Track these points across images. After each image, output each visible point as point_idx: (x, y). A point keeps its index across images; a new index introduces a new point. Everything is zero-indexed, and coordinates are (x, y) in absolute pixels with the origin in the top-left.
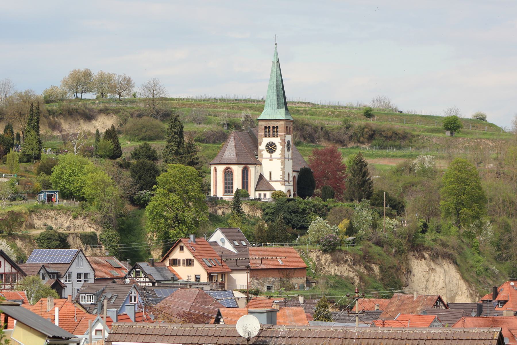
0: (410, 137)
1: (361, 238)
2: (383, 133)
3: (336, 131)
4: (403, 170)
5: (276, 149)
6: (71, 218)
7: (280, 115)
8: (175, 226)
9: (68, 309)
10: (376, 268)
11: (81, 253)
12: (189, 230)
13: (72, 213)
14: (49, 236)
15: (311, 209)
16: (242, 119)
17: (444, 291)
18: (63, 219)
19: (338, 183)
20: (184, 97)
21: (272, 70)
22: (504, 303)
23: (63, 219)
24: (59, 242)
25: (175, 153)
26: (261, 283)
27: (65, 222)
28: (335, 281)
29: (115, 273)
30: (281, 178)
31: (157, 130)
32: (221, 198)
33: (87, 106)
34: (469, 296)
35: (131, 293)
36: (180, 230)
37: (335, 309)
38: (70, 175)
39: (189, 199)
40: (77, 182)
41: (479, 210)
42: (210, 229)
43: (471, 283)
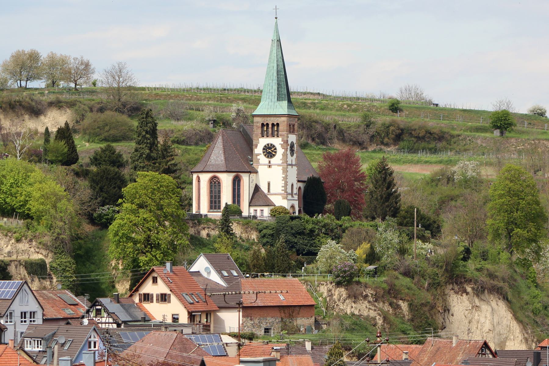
0: (449, 138)
1: (384, 267)
2: (413, 132)
4: (439, 180)
5: (276, 152)
6: (13, 241)
8: (147, 252)
10: (404, 306)
13: (15, 235)
15: (321, 230)
16: (233, 114)
17: (491, 335)
19: (356, 196)
20: (158, 86)
25: (147, 157)
26: (257, 324)
27: (6, 246)
28: (351, 321)
29: (69, 312)
30: (282, 190)
31: (123, 128)
32: (206, 215)
33: (34, 97)
35: (90, 337)
36: (153, 256)
39: (164, 217)
42: (192, 255)
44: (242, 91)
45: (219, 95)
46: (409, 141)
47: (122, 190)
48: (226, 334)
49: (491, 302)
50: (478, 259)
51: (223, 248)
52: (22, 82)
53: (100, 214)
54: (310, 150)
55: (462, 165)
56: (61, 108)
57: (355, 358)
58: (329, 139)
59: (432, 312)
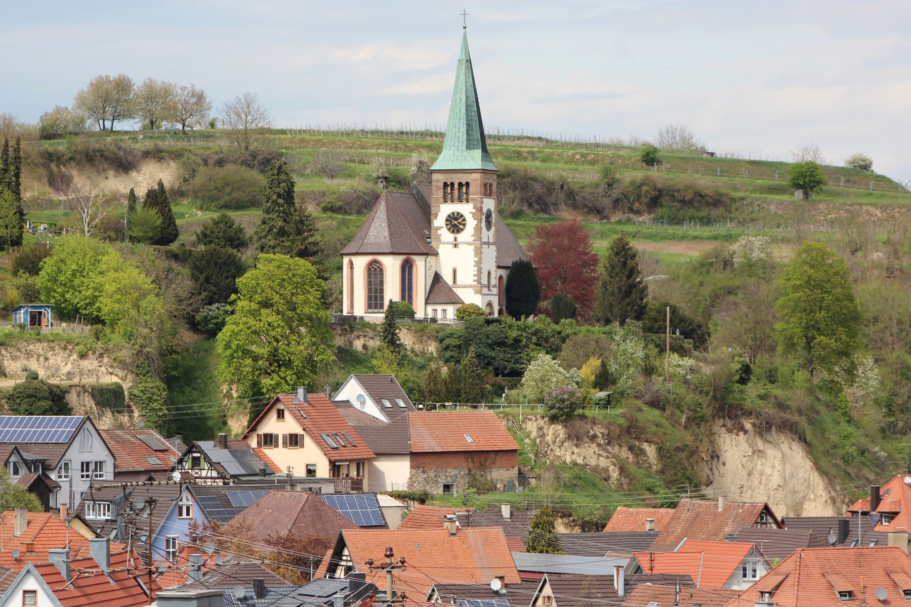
0: (728, 202)
1: (622, 394)
2: (676, 194)
3: (588, 190)
4: (711, 264)
5: (464, 225)
6: (75, 356)
7: (472, 162)
8: (273, 372)
9: (55, 531)
10: (650, 450)
11: (88, 424)
12: (298, 378)
13: (77, 348)
14: (31, 392)
15: (531, 339)
16: (413, 169)
17: (781, 494)
18: (59, 359)
19: (584, 289)
20: (304, 128)
21: (458, 77)
22: (891, 516)
23: (59, 359)
24: (50, 402)
25: (279, 232)
26: (432, 479)
27: (64, 364)
28: (572, 474)
29: (154, 461)
30: (475, 281)
31: (252, 188)
32: (362, 318)
33: (122, 144)
34: (829, 501)
35: (181, 500)
36: (282, 378)
37: (573, 527)
38: (74, 275)
39: (298, 321)
40: (88, 289)
41: (848, 340)
42: (339, 376)
43: (833, 478)
44: (427, 135)
45: (394, 141)
46: (670, 207)
47: (237, 280)
48: (386, 493)
49: (782, 444)
50: (763, 382)
51: (385, 366)
52: (106, 122)
53: (206, 317)
54: (526, 220)
55: (744, 242)
56: (162, 161)
57: (577, 528)
58: (553, 204)
59: (692, 460)
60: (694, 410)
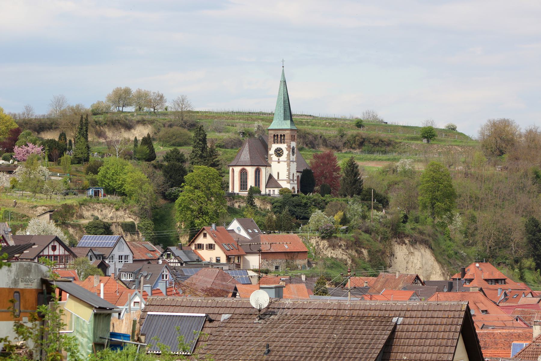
1: (352, 227)
2: (371, 141)
3: (332, 138)
4: (387, 171)
5: (283, 153)
6: (114, 210)
7: (286, 126)
8: (200, 217)
10: (365, 252)
14: (96, 225)
15: (312, 203)
17: (421, 271)
18: (107, 211)
22: (470, 280)
23: (107, 211)
24: (104, 230)
29: (150, 255)
32: (238, 194)
33: (128, 118)
40: (119, 180)
42: (229, 219)
44: (261, 114)
46: (368, 146)
48: (250, 270)
51: (249, 215)
53: (170, 193)
60: (384, 234)
